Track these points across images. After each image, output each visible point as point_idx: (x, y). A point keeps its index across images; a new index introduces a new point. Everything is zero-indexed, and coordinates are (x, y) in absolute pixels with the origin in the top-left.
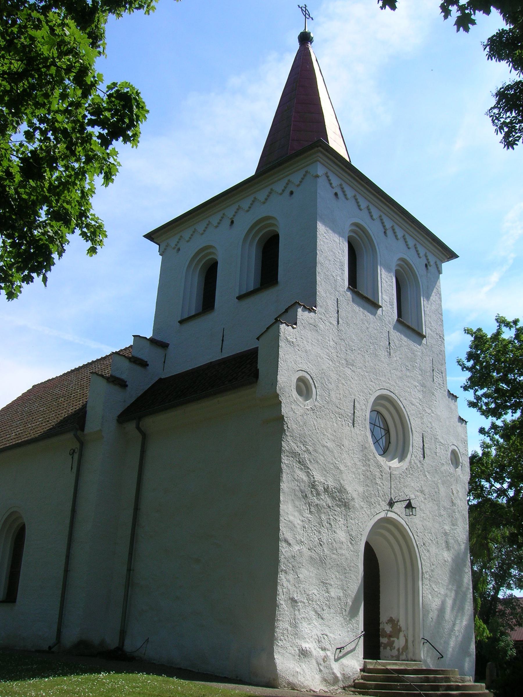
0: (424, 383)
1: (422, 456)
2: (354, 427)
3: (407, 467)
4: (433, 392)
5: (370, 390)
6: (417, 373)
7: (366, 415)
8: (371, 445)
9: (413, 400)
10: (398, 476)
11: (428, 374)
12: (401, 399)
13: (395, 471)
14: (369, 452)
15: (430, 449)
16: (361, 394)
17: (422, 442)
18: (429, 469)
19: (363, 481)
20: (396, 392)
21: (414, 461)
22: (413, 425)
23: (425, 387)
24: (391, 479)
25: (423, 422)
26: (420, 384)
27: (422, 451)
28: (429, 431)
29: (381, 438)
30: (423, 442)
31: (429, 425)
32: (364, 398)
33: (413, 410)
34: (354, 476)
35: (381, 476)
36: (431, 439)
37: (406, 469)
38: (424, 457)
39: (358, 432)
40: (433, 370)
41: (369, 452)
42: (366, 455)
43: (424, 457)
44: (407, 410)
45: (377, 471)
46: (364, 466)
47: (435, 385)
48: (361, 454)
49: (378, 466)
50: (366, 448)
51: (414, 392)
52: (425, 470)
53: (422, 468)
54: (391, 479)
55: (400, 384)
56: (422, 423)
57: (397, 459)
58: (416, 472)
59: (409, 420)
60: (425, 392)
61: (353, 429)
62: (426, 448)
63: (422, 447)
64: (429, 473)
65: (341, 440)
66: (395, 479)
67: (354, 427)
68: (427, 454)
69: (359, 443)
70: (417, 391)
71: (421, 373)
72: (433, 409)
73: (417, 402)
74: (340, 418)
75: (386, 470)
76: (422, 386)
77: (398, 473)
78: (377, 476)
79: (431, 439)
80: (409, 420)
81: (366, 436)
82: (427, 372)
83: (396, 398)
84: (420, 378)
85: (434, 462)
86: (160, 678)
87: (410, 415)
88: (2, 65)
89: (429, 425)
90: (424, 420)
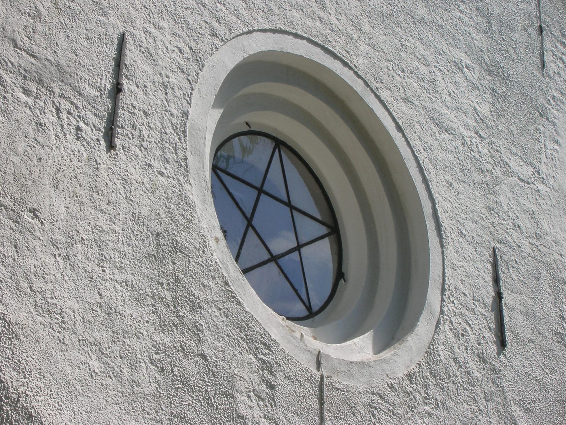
0: (496, 64)
1: (490, 336)
2: (111, 146)
3: (413, 367)
4: (543, 108)
5: (219, 21)
6: (466, 19)
7: (186, 115)
8: (211, 242)
9: (445, 111)
10: (365, 399)
11: (516, 36)
12: (385, 94)
13: (350, 375)
14: (198, 269)
15: (530, 315)
16: (165, 24)
17: (489, 279)
18: (529, 396)
19: (157, 397)
20: (360, 62)
21: (451, 348)
22: (447, 205)
23: (505, 79)
24: (321, 409)
25: (494, 205)
26: (481, 62)
27: (491, 316)
28: (527, 248)
29: (250, 224)
30: (496, 280)
31: (526, 223)
32: (181, 45)
33: (444, 150)
34: (95, 364)
35: (264, 387)
36: (537, 279)
37: (410, 376)
38: (502, 343)
39: (135, 174)
40: (541, 30)
41: (198, 269)
42: (177, 279)
43: (502, 343)
44: (416, 143)
45: (241, 364)
46: (163, 327)
47: (552, 85)
48: (152, 272)
49: (249, 339)
50: (176, 249)
51: (451, 87)
52: (509, 395)
53: (494, 388)
54: (321, 409)
55: (380, 39)
56: (489, 209)
57: (372, 331)
58: (459, 399)
59: (425, 181)
60: (505, 97)
61: (105, 156)
62: (512, 309)
63: (489, 301)
64: (528, 411)
65: (23, 186)
66: (345, 409)
67: (111, 146)
68: (516, 335)
69: (136, 219)
70: (463, 84)
71: (484, 25)
72: (543, 169)
73: (466, 125)
74: (26, 92)
75: (298, 364)
76: (490, 73)
77: (362, 388)
78: (241, 385)
79: (537, 279)
80: (425, 181)
81: (183, 198)
82: (513, 29)
83: (358, 86)
84: (479, 40)
85: (553, 371)
86: (227, 249)
87: (426, 164)
88: (485, 424)
89: (526, 223)
90: (502, 199)
